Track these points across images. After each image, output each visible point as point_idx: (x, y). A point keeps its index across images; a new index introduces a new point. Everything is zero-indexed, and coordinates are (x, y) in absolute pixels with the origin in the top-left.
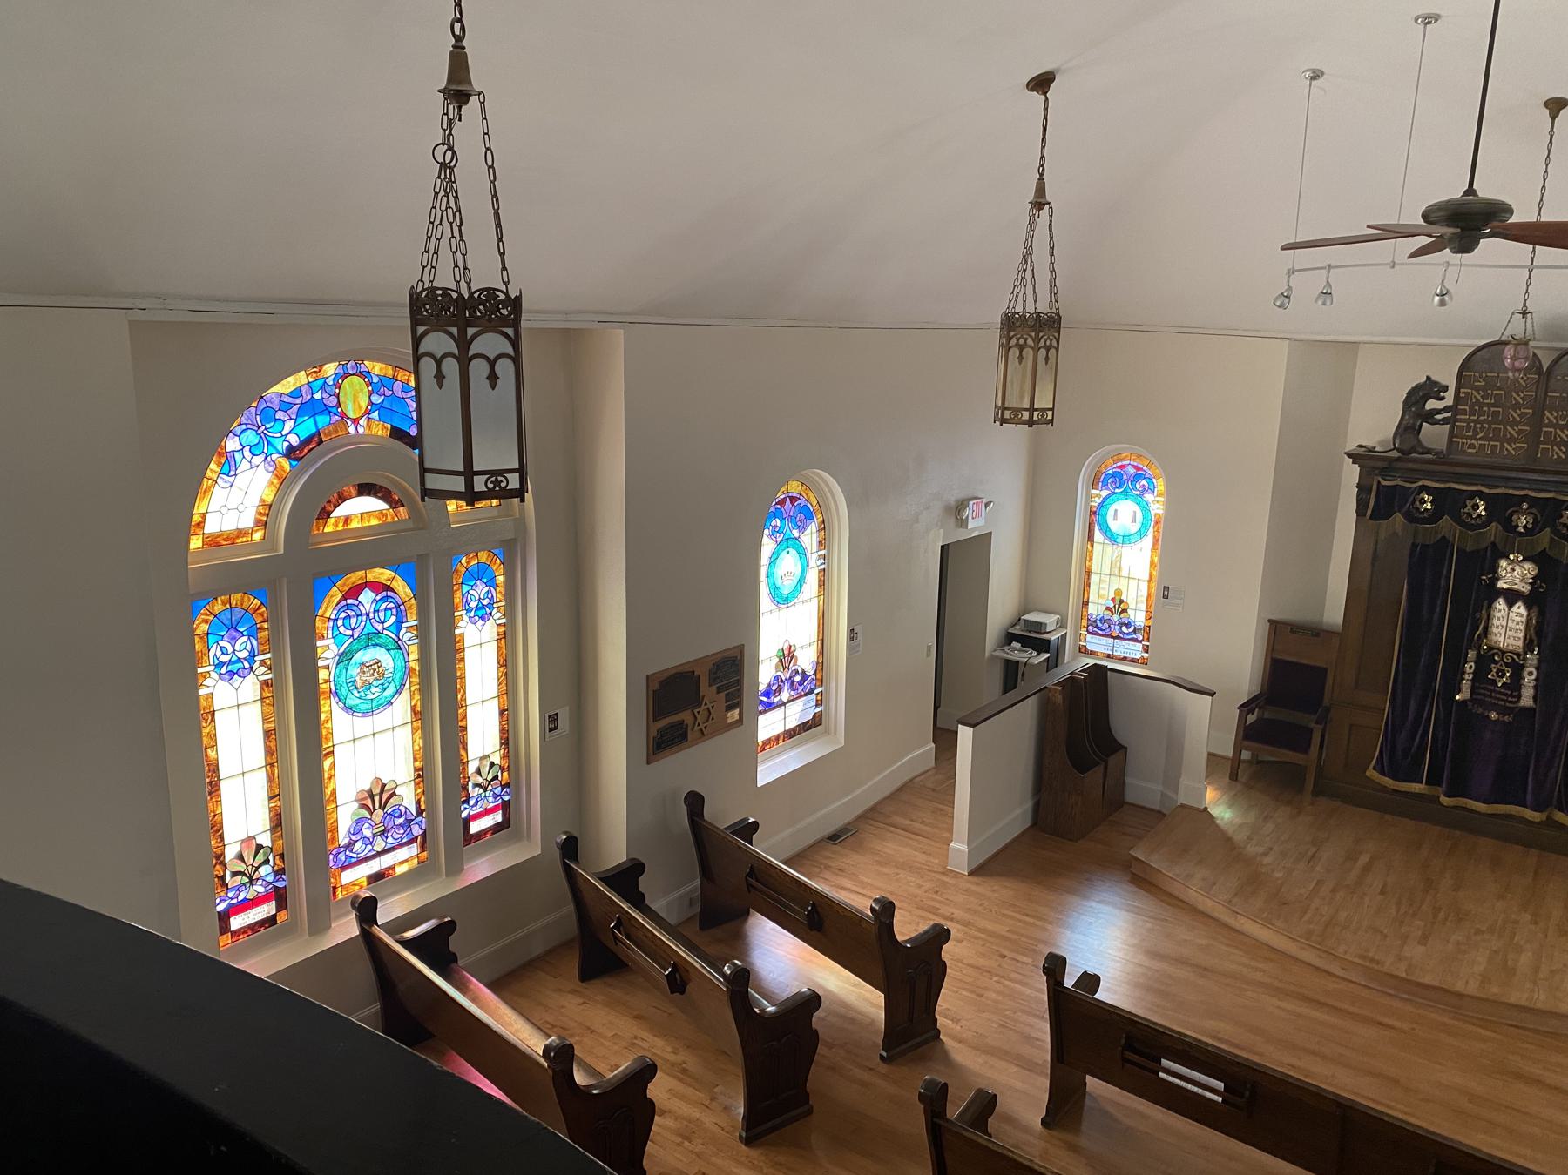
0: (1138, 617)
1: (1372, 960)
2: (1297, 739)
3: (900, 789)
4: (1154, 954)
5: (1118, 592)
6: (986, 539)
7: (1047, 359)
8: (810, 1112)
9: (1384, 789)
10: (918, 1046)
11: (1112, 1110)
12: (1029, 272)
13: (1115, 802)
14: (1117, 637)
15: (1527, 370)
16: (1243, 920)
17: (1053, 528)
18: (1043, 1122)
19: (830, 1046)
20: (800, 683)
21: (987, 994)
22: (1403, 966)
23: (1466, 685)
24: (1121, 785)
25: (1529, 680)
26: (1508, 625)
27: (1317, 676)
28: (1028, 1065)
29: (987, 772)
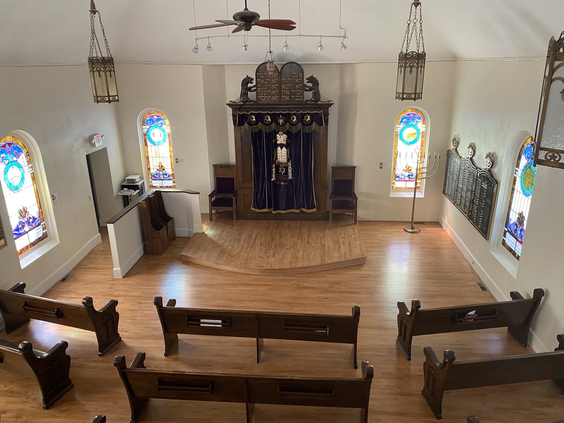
0: (169, 171)
1: (261, 266)
2: (229, 203)
3: (89, 254)
4: (194, 285)
5: (160, 163)
6: (104, 151)
7: (111, 76)
8: (73, 386)
9: (256, 213)
10: (112, 347)
11: (188, 342)
12: (95, 40)
13: (173, 238)
15: (274, 72)
16: (221, 266)
17: (130, 144)
18: (165, 355)
19: (77, 359)
20: (33, 222)
21: (137, 318)
22: (269, 266)
23: (274, 175)
24: (174, 231)
25: (290, 171)
26: (282, 155)
27: (231, 181)
28: (156, 338)
29: (123, 238)
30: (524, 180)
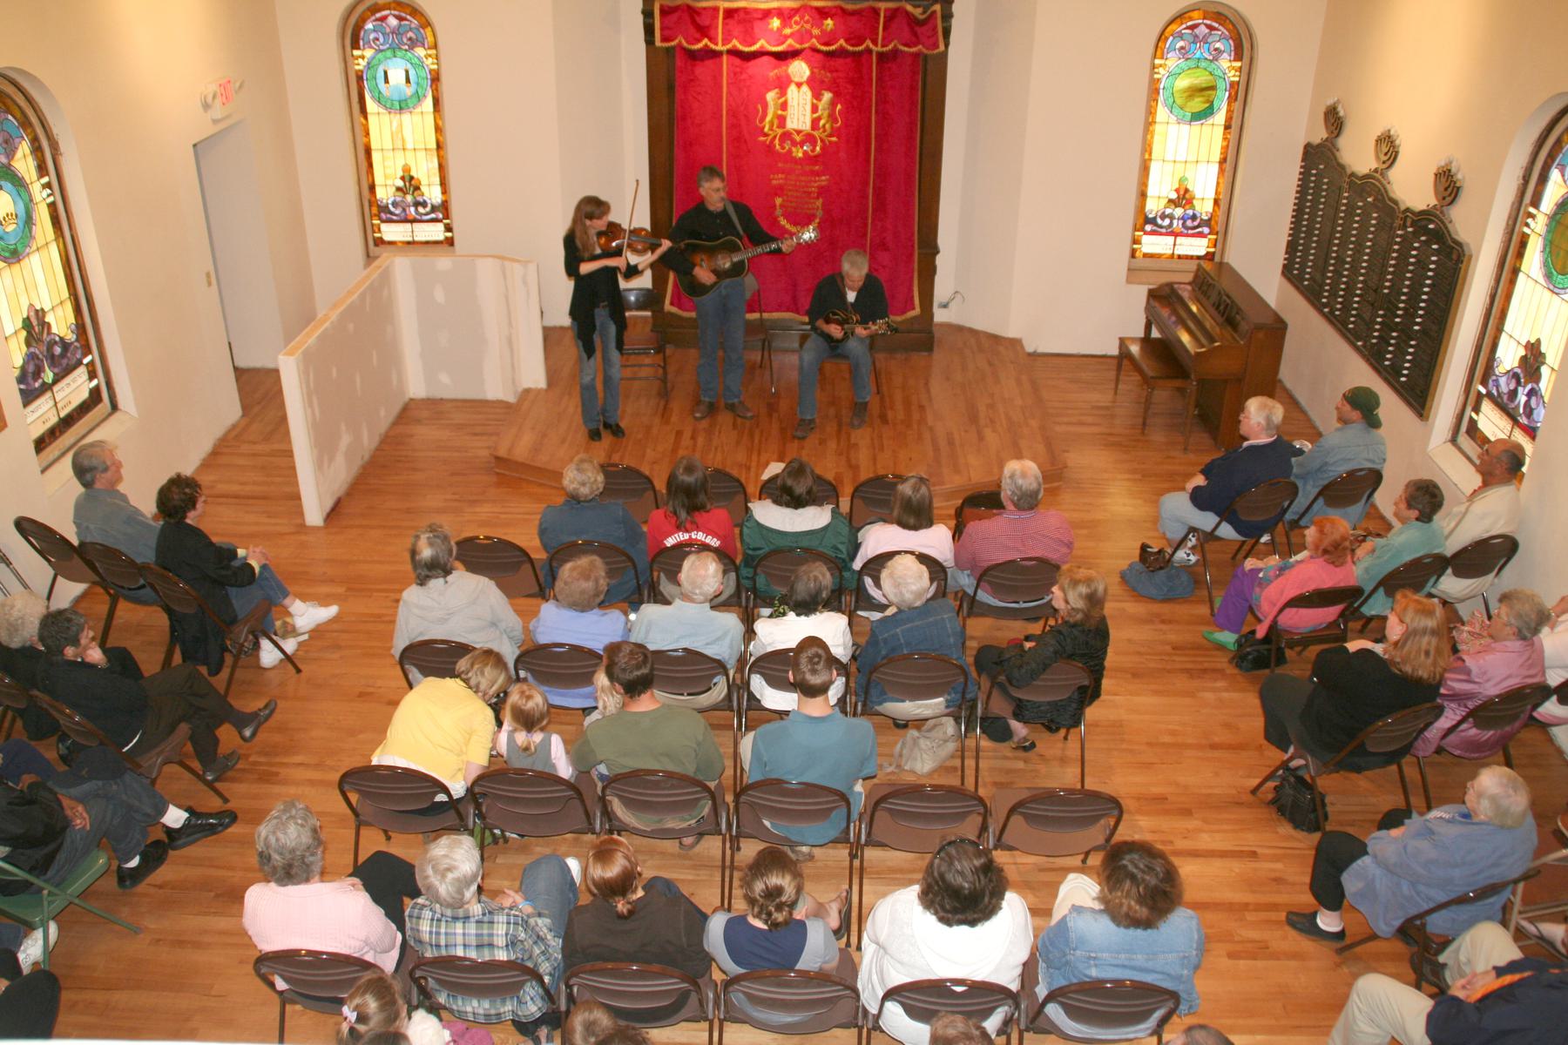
5: (406, 169)
14: (1181, 234)
20: (63, 355)
30: (1551, 247)
